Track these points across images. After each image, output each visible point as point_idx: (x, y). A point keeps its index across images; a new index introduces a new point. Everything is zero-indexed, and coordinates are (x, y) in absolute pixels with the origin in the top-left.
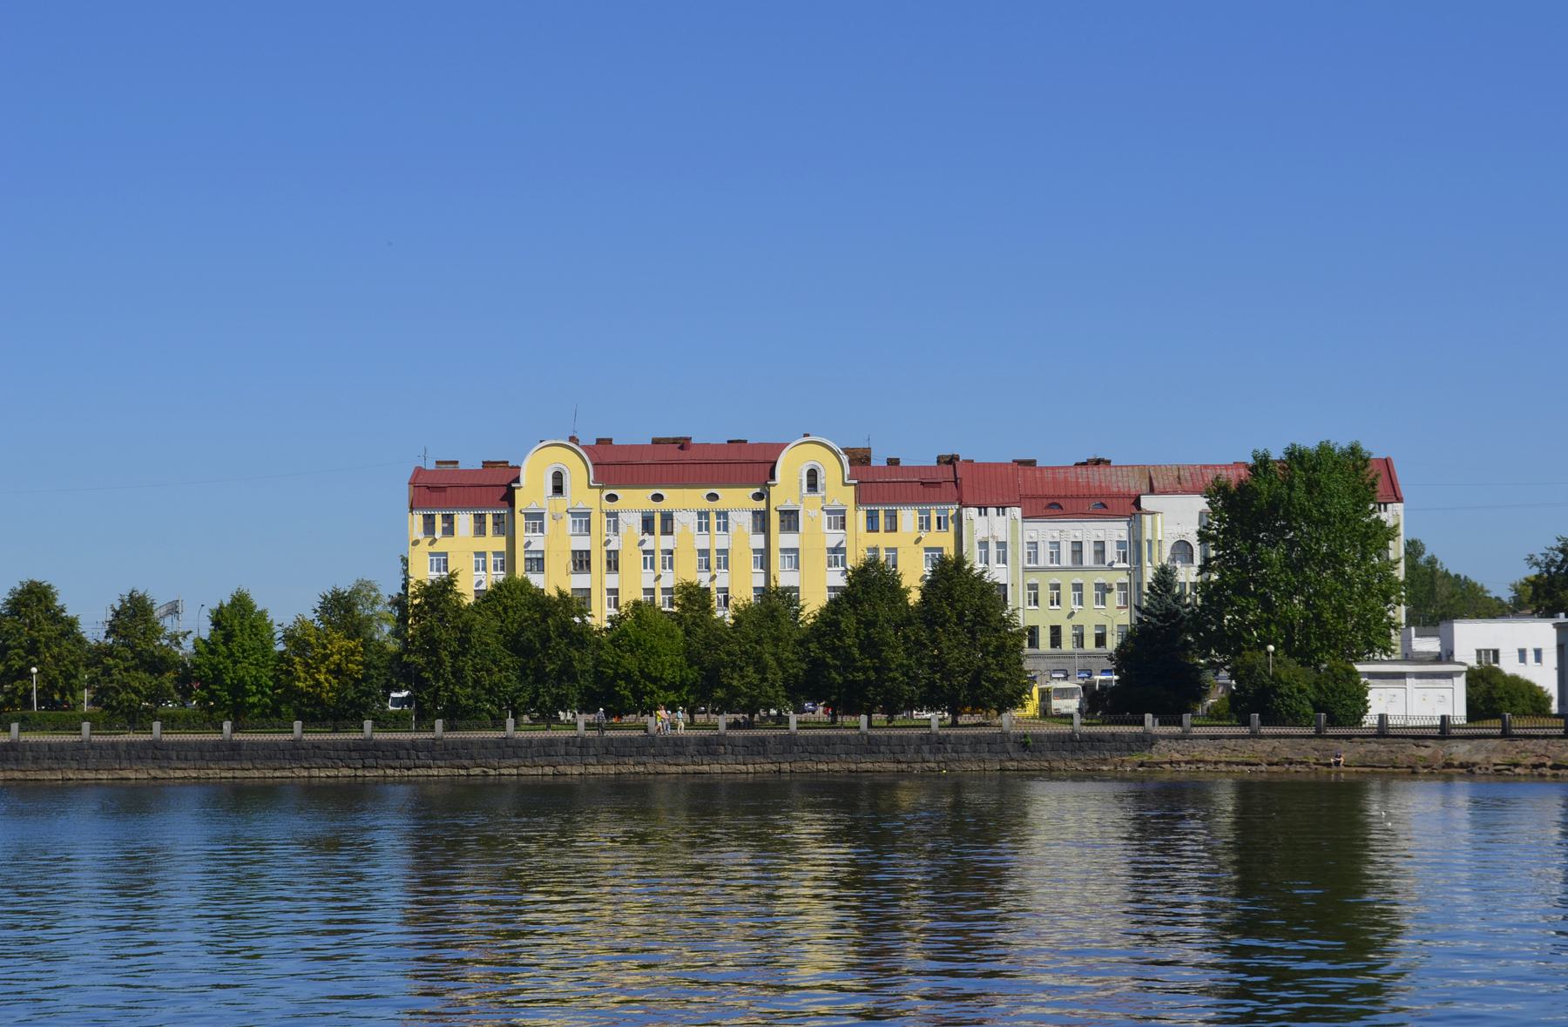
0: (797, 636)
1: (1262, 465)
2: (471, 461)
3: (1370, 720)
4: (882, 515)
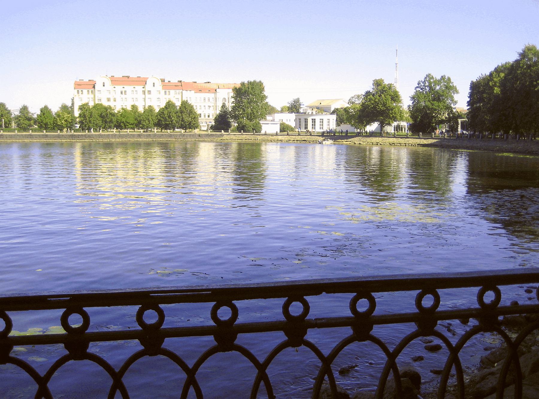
0: (156, 115)
1: (243, 84)
2: (86, 80)
3: (263, 132)
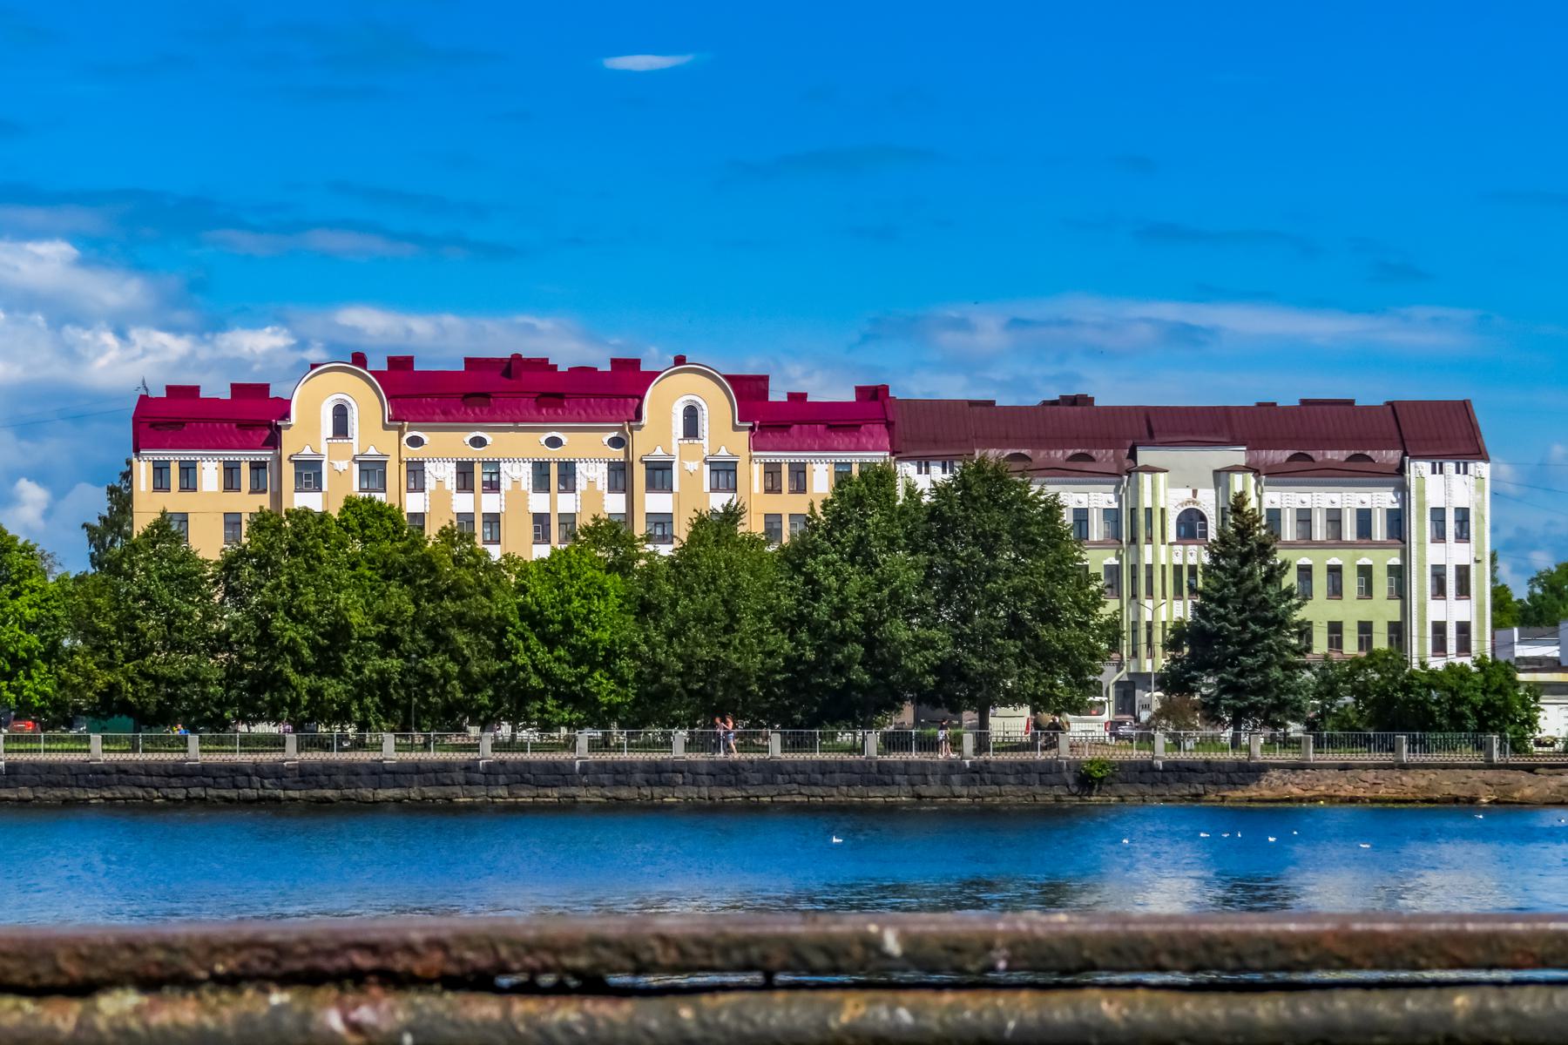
4: (175, 468)
